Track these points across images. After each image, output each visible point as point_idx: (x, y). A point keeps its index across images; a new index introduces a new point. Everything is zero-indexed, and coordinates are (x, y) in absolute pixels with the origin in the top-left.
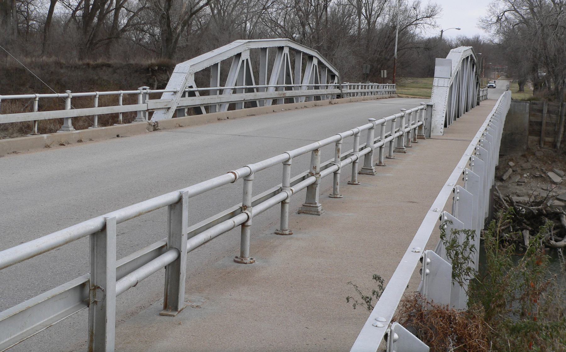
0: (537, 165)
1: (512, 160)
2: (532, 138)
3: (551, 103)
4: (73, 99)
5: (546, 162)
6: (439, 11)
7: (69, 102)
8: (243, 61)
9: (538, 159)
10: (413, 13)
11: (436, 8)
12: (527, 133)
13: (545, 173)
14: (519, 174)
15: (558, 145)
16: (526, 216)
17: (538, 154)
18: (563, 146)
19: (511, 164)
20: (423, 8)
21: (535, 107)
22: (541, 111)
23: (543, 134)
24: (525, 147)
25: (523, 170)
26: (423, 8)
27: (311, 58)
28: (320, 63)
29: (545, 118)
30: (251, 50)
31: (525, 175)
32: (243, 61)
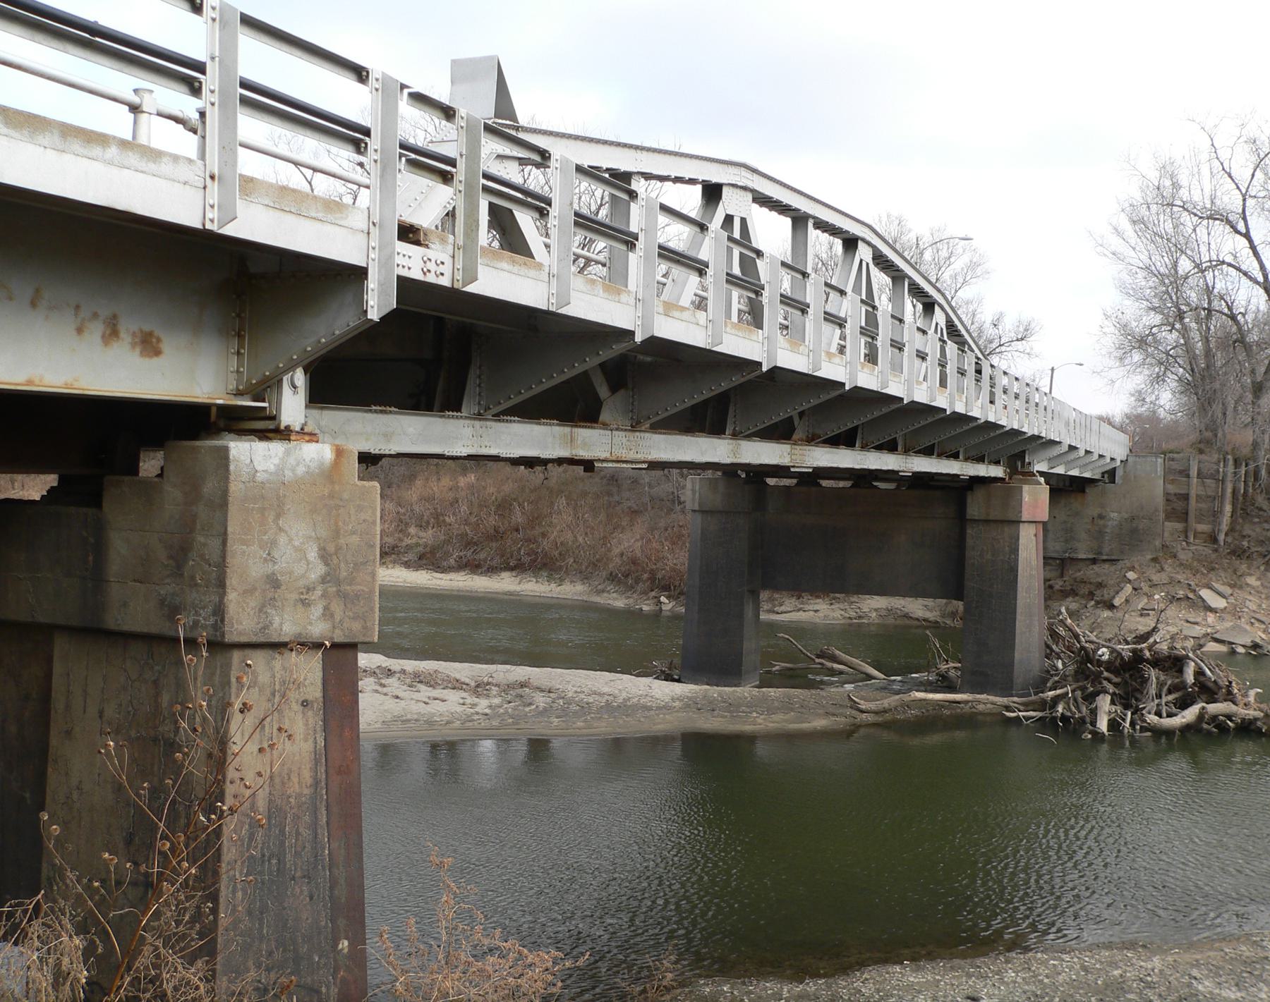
0: (1180, 577)
1: (1132, 569)
3: (1203, 457)
5: (1197, 571)
6: (1037, 329)
9: (1181, 564)
10: (990, 332)
11: (1033, 325)
12: (1162, 516)
14: (1146, 594)
15: (1221, 537)
16: (1109, 666)
17: (1182, 556)
18: (1229, 539)
20: (1008, 328)
21: (1175, 465)
22: (1185, 473)
24: (1158, 543)
25: (1153, 586)
31: (1157, 597)
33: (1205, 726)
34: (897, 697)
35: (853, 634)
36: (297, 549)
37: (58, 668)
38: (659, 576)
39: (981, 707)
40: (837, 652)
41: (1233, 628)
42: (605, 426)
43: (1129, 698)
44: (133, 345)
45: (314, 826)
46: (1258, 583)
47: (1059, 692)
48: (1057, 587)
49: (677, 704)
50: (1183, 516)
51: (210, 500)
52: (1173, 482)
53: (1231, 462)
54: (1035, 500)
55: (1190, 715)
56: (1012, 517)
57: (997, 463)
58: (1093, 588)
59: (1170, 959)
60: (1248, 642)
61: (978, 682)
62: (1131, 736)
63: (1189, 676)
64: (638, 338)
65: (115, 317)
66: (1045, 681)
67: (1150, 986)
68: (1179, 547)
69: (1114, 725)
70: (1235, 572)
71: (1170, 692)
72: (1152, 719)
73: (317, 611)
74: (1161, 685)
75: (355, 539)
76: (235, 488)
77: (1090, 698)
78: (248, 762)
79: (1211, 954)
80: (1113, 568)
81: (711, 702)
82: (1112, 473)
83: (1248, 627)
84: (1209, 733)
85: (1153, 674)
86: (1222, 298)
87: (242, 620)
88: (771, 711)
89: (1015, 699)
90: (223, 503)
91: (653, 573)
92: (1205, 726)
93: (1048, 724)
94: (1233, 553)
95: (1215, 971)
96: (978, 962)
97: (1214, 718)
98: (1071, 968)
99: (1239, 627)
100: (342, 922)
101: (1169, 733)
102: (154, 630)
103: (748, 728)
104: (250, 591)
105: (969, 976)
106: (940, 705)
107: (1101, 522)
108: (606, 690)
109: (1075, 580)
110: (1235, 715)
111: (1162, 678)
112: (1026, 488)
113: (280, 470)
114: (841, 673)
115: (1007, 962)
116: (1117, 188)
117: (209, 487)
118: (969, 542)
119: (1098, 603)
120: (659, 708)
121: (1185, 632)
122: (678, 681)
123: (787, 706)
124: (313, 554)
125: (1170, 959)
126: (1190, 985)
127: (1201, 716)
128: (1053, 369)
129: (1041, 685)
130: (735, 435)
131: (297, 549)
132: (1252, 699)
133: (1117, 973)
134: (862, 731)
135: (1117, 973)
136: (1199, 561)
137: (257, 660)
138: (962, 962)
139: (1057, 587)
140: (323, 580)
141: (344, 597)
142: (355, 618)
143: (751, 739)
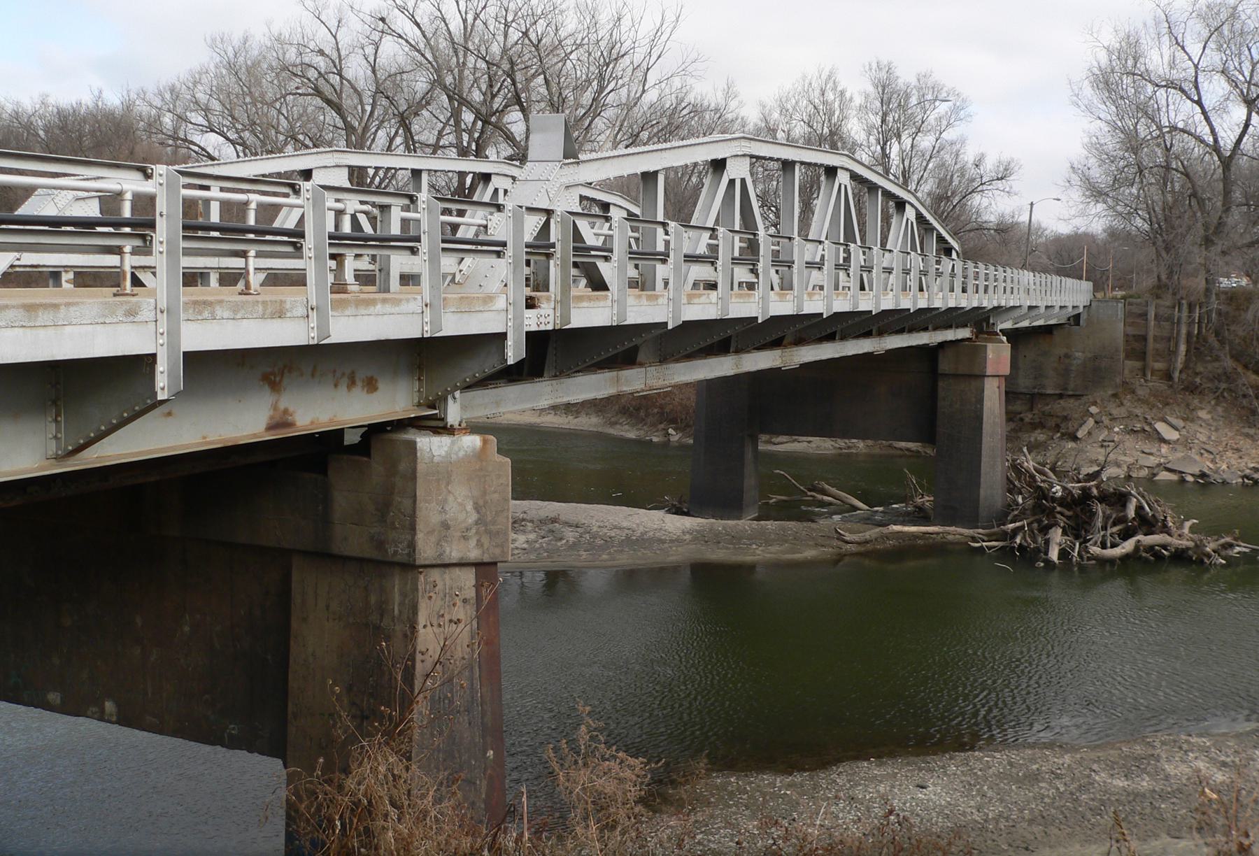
0: (1138, 411)
1: (1095, 403)
2: (1130, 364)
3: (1159, 301)
5: (1153, 406)
8: (732, 182)
11: (1012, 165)
12: (1122, 356)
13: (1150, 424)
15: (1176, 374)
16: (1062, 502)
17: (1140, 392)
18: (1184, 376)
19: (1093, 409)
20: (989, 166)
21: (1135, 309)
22: (1144, 315)
23: (1149, 358)
24: (1118, 380)
25: (1113, 419)
26: (989, 166)
31: (1116, 429)
32: (732, 182)
33: (1144, 555)
34: (878, 530)
35: (839, 466)
36: (460, 504)
37: (295, 577)
38: (667, 410)
39: (950, 537)
40: (827, 487)
41: (1184, 458)
42: (641, 365)
43: (1079, 529)
44: (363, 387)
45: (471, 679)
46: (1209, 416)
47: (1018, 524)
48: (1027, 420)
49: (687, 537)
50: (1142, 356)
51: (404, 473)
52: (1132, 324)
53: (1185, 307)
54: (998, 356)
55: (1128, 546)
56: (977, 372)
57: (965, 326)
58: (1059, 421)
59: (1078, 756)
60: (1196, 471)
61: (948, 515)
62: (1078, 564)
63: (1131, 512)
64: (670, 327)
65: (353, 372)
66: (1007, 514)
67: (1058, 777)
68: (1138, 382)
69: (1064, 554)
70: (1188, 405)
71: (1114, 524)
72: (1095, 550)
73: (473, 543)
74: (1106, 518)
75: (496, 496)
76: (421, 467)
77: (1045, 530)
78: (428, 639)
79: (1112, 752)
80: (1077, 403)
81: (717, 534)
82: (1077, 317)
83: (1197, 458)
84: (1146, 560)
85: (1099, 509)
86: (1177, 158)
87: (426, 550)
88: (768, 542)
89: (980, 531)
90: (413, 476)
91: (662, 407)
92: (1144, 555)
93: (1006, 553)
94: (1186, 389)
95: (1111, 766)
96: (928, 759)
97: (1150, 549)
98: (1000, 764)
99: (1190, 457)
100: (489, 739)
101: (1111, 561)
102: (367, 555)
103: (749, 559)
104: (431, 532)
105: (920, 769)
106: (914, 536)
107: (1067, 361)
108: (625, 524)
109: (1043, 413)
110: (1170, 545)
111: (1108, 512)
112: (990, 346)
113: (448, 454)
114: (830, 504)
115: (951, 758)
116: (1086, 52)
117: (403, 466)
118: (941, 393)
119: (1063, 435)
120: (672, 541)
121: (1140, 462)
122: (687, 514)
123: (782, 539)
124: (469, 507)
125: (1078, 756)
126: (1089, 776)
127: (1137, 548)
128: (1032, 204)
129: (1002, 518)
130: (737, 351)
131: (460, 504)
132: (1186, 531)
133: (1035, 767)
134: (847, 559)
135: (1035, 767)
136: (1155, 396)
137: (435, 574)
138: (916, 759)
139: (1027, 420)
140: (477, 523)
141: (489, 532)
142: (497, 546)
143: (751, 567)
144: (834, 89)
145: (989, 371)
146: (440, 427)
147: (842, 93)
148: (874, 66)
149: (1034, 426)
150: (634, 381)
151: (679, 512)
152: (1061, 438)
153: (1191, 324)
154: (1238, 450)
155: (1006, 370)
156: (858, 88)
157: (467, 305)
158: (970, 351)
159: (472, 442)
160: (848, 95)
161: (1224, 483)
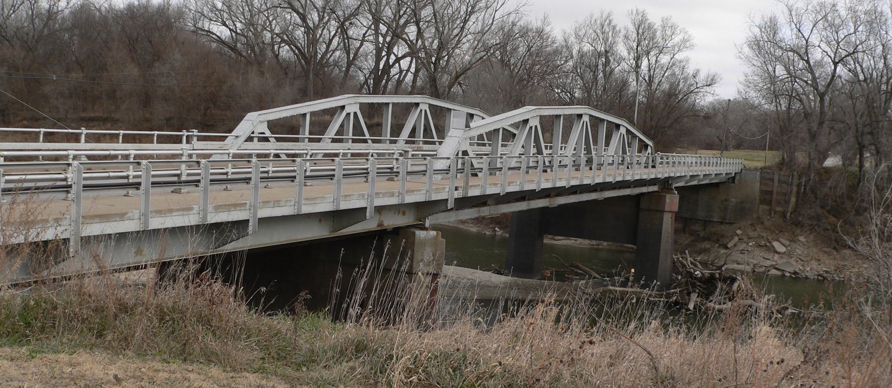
1: (740, 228)
4: (124, 135)
7: (83, 137)
8: (531, 128)
9: (765, 228)
12: (758, 201)
15: (788, 215)
16: (700, 280)
17: (767, 223)
19: (739, 232)
20: (702, 77)
22: (772, 180)
23: (773, 203)
24: (755, 216)
25: (749, 238)
26: (702, 77)
27: (618, 126)
28: (628, 131)
29: (776, 187)
30: (361, 104)
32: (531, 128)
48: (701, 235)
51: (411, 244)
70: (793, 233)
82: (734, 178)
83: (794, 263)
90: (414, 243)
112: (668, 196)
121: (761, 264)
139: (701, 235)
144: (609, 24)
145: (667, 209)
146: (423, 228)
147: (614, 27)
148: (635, 12)
149: (705, 239)
150: (485, 211)
151: (499, 273)
152: (719, 247)
153: (799, 185)
154: (819, 260)
155: (676, 209)
156: (624, 23)
157: (437, 191)
158: (656, 199)
159: (433, 233)
160: (618, 28)
161: (807, 278)
